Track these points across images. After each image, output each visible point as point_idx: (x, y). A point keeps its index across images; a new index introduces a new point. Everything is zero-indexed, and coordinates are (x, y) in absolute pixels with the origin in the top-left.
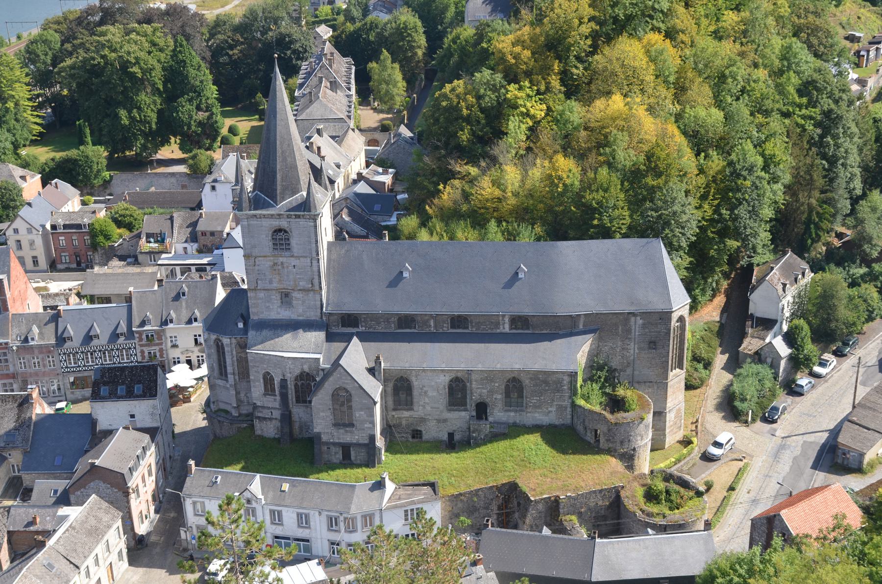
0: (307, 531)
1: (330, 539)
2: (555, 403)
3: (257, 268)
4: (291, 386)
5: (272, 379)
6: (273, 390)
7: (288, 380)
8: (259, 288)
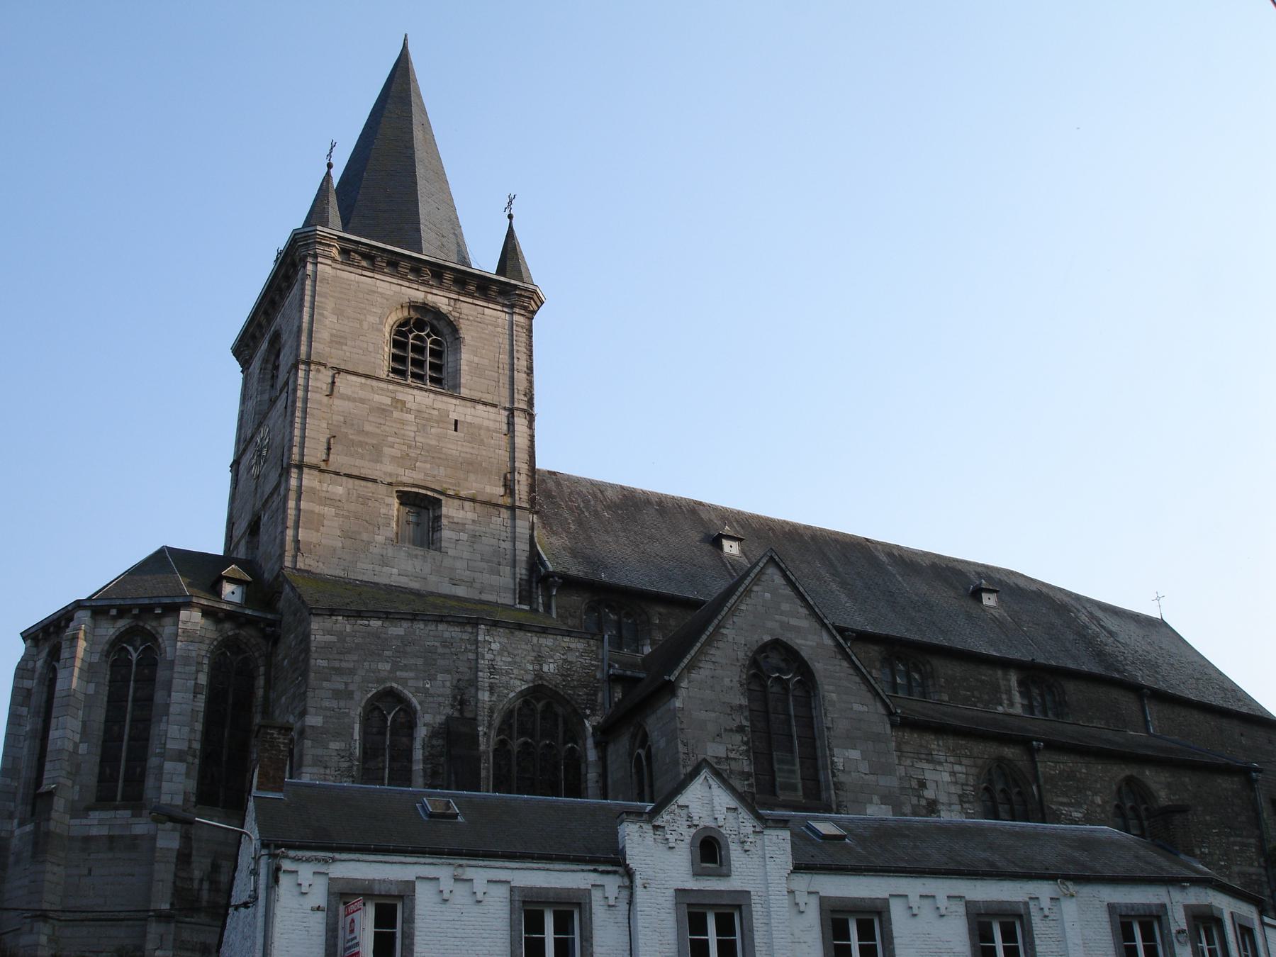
2: (1235, 869)
7: (483, 716)
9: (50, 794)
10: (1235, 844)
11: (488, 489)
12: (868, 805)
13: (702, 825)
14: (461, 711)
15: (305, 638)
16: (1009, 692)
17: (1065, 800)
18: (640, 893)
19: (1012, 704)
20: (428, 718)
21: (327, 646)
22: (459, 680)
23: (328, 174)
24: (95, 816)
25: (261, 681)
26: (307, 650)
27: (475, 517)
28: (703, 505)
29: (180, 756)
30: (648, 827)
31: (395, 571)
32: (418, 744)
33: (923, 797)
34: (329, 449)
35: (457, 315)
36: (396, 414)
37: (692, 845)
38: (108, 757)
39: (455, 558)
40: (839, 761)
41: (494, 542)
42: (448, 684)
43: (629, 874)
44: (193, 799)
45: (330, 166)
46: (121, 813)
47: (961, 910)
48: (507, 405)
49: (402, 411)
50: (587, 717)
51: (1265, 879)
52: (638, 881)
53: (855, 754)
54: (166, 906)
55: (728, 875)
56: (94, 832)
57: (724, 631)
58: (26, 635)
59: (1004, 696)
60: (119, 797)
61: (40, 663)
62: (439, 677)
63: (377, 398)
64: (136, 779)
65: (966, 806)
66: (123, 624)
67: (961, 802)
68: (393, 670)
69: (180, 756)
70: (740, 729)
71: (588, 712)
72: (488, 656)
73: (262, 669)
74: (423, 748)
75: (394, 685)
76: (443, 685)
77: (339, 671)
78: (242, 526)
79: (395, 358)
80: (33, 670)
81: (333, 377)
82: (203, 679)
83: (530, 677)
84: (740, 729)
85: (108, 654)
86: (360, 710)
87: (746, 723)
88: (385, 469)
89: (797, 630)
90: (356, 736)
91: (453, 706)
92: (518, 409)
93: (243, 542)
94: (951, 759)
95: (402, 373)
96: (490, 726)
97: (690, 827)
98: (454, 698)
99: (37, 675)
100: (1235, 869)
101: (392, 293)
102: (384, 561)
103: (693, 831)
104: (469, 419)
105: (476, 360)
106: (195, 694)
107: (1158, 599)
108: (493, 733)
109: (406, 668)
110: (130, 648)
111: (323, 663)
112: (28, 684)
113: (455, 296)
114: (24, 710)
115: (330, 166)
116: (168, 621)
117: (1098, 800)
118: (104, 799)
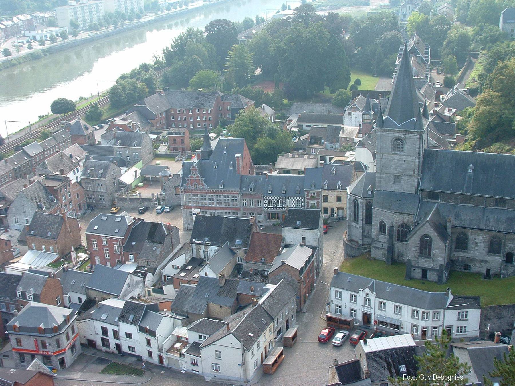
5: (385, 226)
11: (410, 173)
21: (374, 213)
27: (408, 178)
36: (394, 161)
39: (404, 186)
40: (434, 252)
41: (411, 182)
63: (390, 158)
68: (383, 218)
70: (418, 246)
76: (390, 221)
84: (418, 246)
88: (392, 171)
89: (431, 233)
102: (392, 187)
104: (407, 160)
109: (385, 218)
113: (405, 134)
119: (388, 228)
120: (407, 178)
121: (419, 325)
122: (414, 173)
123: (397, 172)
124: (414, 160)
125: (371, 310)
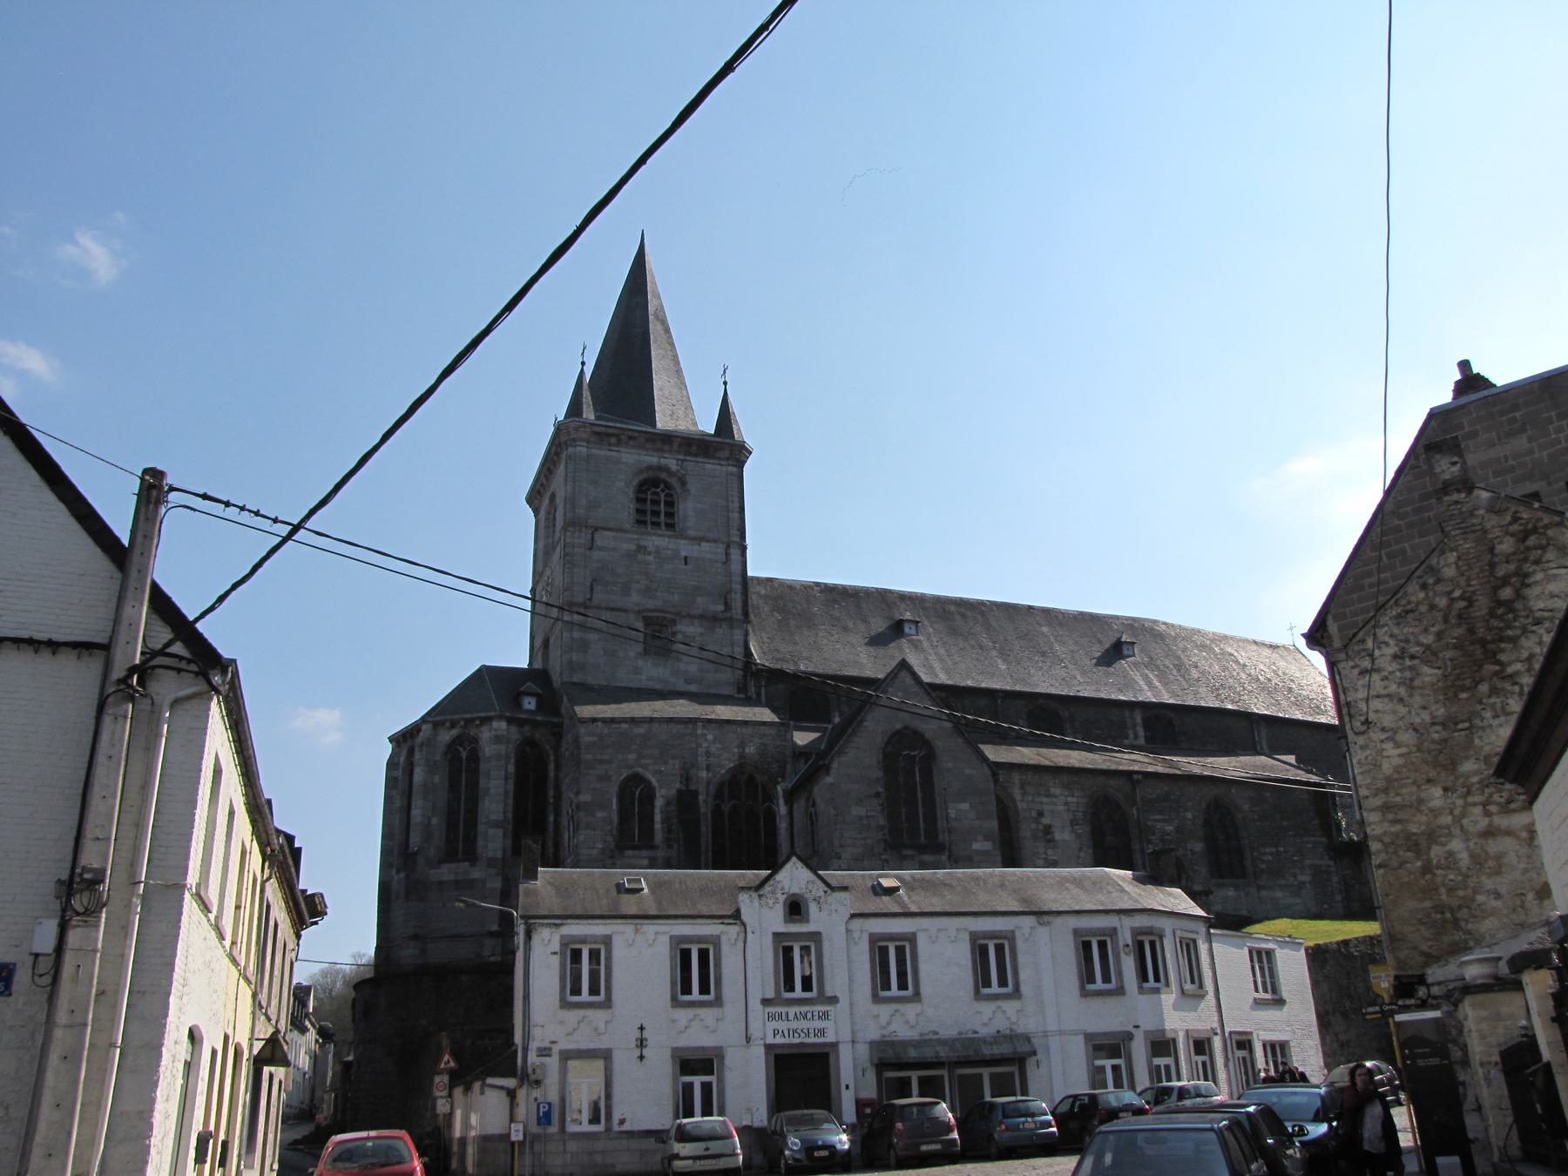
0: (1010, 1007)
1: (1091, 1029)
2: (1308, 862)
3: (596, 554)
4: (705, 805)
5: (649, 796)
6: (647, 832)
7: (702, 789)
8: (595, 602)
9: (415, 854)
10: (1307, 843)
12: (973, 843)
13: (792, 892)
14: (687, 785)
15: (577, 740)
16: (1134, 726)
17: (1161, 817)
18: (750, 936)
19: (1136, 737)
20: (664, 792)
22: (685, 763)
23: (582, 370)
24: (445, 867)
25: (552, 766)
26: (578, 748)
28: (893, 593)
29: (498, 825)
30: (755, 895)
31: (644, 677)
32: (657, 811)
33: (1041, 823)
34: (592, 590)
35: (684, 472)
36: (640, 557)
37: (784, 905)
38: (451, 824)
42: (677, 767)
43: (744, 924)
44: (509, 852)
45: (583, 364)
46: (462, 864)
47: (967, 937)
48: (725, 540)
49: (644, 554)
50: (779, 783)
51: (1333, 869)
52: (749, 930)
53: (965, 806)
54: (495, 928)
55: (808, 921)
56: (445, 878)
57: (865, 724)
58: (391, 739)
59: (1130, 732)
60: (460, 853)
61: (402, 759)
62: (671, 762)
63: (625, 546)
64: (471, 840)
65: (1076, 827)
66: (455, 732)
67: (1072, 825)
69: (498, 825)
70: (878, 795)
71: (779, 780)
72: (705, 745)
73: (552, 758)
74: (661, 813)
75: (640, 770)
77: (601, 762)
78: (538, 643)
79: (638, 511)
80: (398, 763)
81: (593, 534)
82: (511, 768)
83: (736, 757)
84: (878, 795)
85: (446, 754)
86: (616, 788)
87: (880, 790)
90: (614, 807)
91: (681, 782)
92: (733, 542)
93: (540, 654)
94: (1066, 793)
95: (644, 523)
96: (707, 794)
97: (783, 894)
98: (682, 776)
99: (401, 767)
100: (1308, 862)
101: (633, 461)
103: (785, 896)
104: (695, 555)
105: (700, 506)
106: (506, 779)
107: (1291, 628)
108: (710, 800)
110: (461, 749)
111: (589, 757)
112: (395, 774)
113: (681, 457)
114: (394, 792)
115: (583, 364)
116: (485, 728)
117: (1189, 815)
118: (450, 856)
119: (668, 804)
120: (699, 630)
121: (1129, 1037)
122: (728, 607)
123: (659, 603)
124: (724, 558)
125: (825, 1016)
